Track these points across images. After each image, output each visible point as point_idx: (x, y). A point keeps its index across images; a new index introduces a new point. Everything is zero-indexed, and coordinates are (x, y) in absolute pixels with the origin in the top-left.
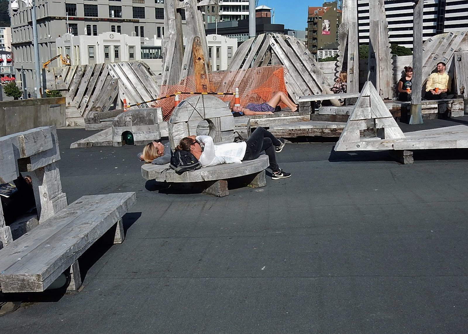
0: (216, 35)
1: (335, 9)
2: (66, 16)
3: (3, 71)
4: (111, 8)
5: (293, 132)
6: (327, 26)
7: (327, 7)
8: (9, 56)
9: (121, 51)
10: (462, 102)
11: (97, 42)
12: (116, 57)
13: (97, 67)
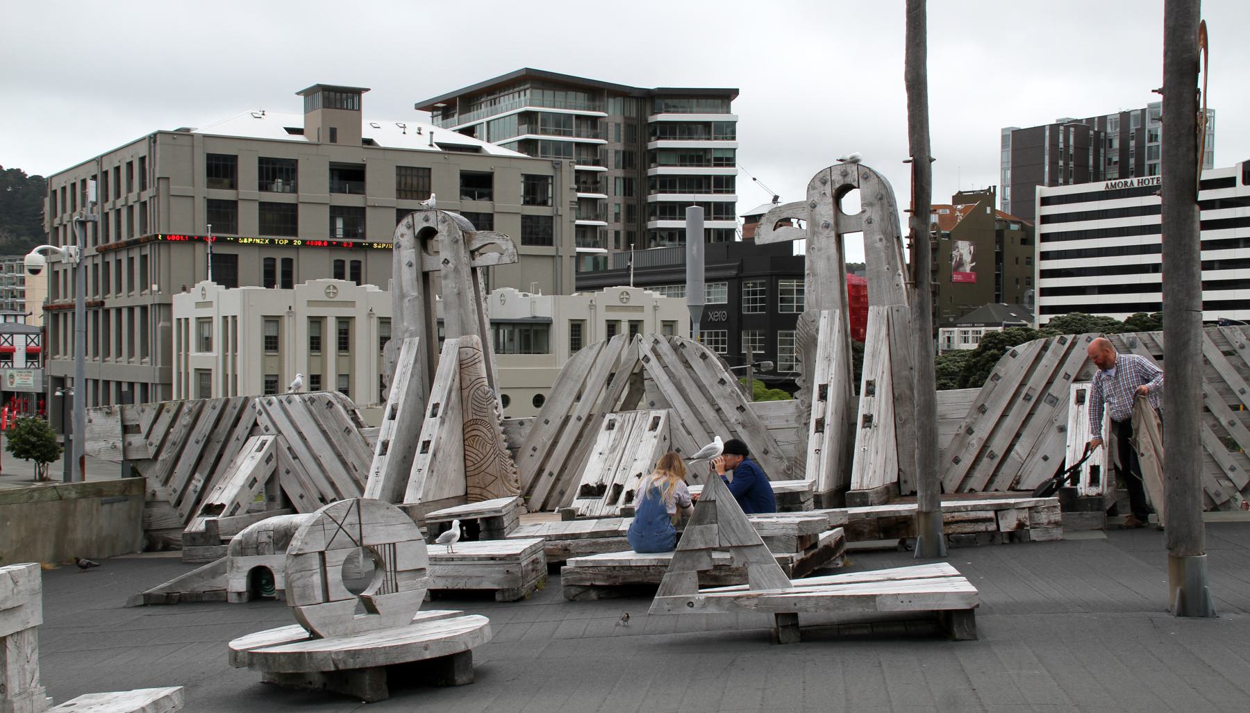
0: (630, 289)
1: (988, 210)
2: (205, 235)
3: (12, 383)
4: (336, 211)
5: (615, 573)
6: (967, 258)
7: (964, 205)
8: (36, 340)
9: (334, 342)
10: (1055, 507)
11: (290, 307)
12: (340, 348)
13: (229, 408)
